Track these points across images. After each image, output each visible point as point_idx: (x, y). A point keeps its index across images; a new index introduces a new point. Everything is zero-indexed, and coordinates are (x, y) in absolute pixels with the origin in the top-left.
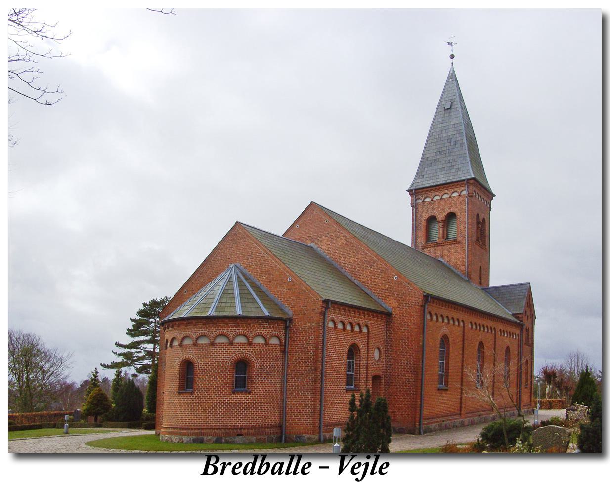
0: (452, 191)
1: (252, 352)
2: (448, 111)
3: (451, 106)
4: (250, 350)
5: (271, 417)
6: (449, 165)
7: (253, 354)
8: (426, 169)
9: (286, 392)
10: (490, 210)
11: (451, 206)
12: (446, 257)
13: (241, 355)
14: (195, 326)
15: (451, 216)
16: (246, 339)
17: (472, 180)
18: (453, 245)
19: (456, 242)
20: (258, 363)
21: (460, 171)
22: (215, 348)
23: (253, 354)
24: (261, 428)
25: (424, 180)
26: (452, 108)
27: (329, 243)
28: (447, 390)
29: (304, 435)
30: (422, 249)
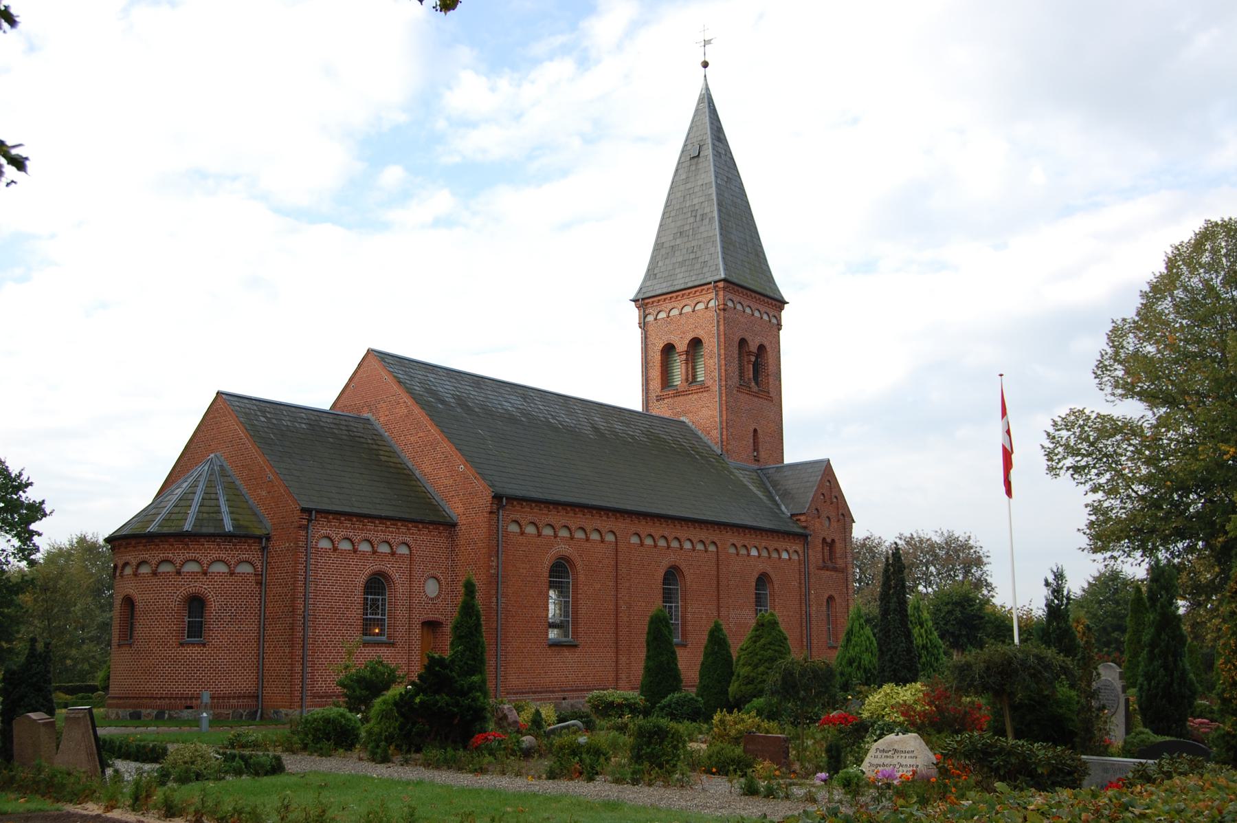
0: (695, 302)
1: (208, 585)
2: (696, 159)
3: (699, 153)
4: (206, 581)
5: (244, 682)
6: (692, 256)
7: (210, 588)
8: (660, 264)
9: (263, 644)
10: (780, 329)
11: (696, 327)
12: (691, 415)
13: (192, 590)
14: (134, 547)
15: (696, 343)
16: (569, 533)
17: (722, 283)
18: (700, 394)
19: (704, 388)
20: (218, 602)
21: (706, 266)
22: (158, 579)
23: (210, 588)
24: (224, 698)
25: (655, 282)
26: (701, 155)
27: (387, 413)
28: (576, 646)
29: (281, 710)
30: (657, 400)
